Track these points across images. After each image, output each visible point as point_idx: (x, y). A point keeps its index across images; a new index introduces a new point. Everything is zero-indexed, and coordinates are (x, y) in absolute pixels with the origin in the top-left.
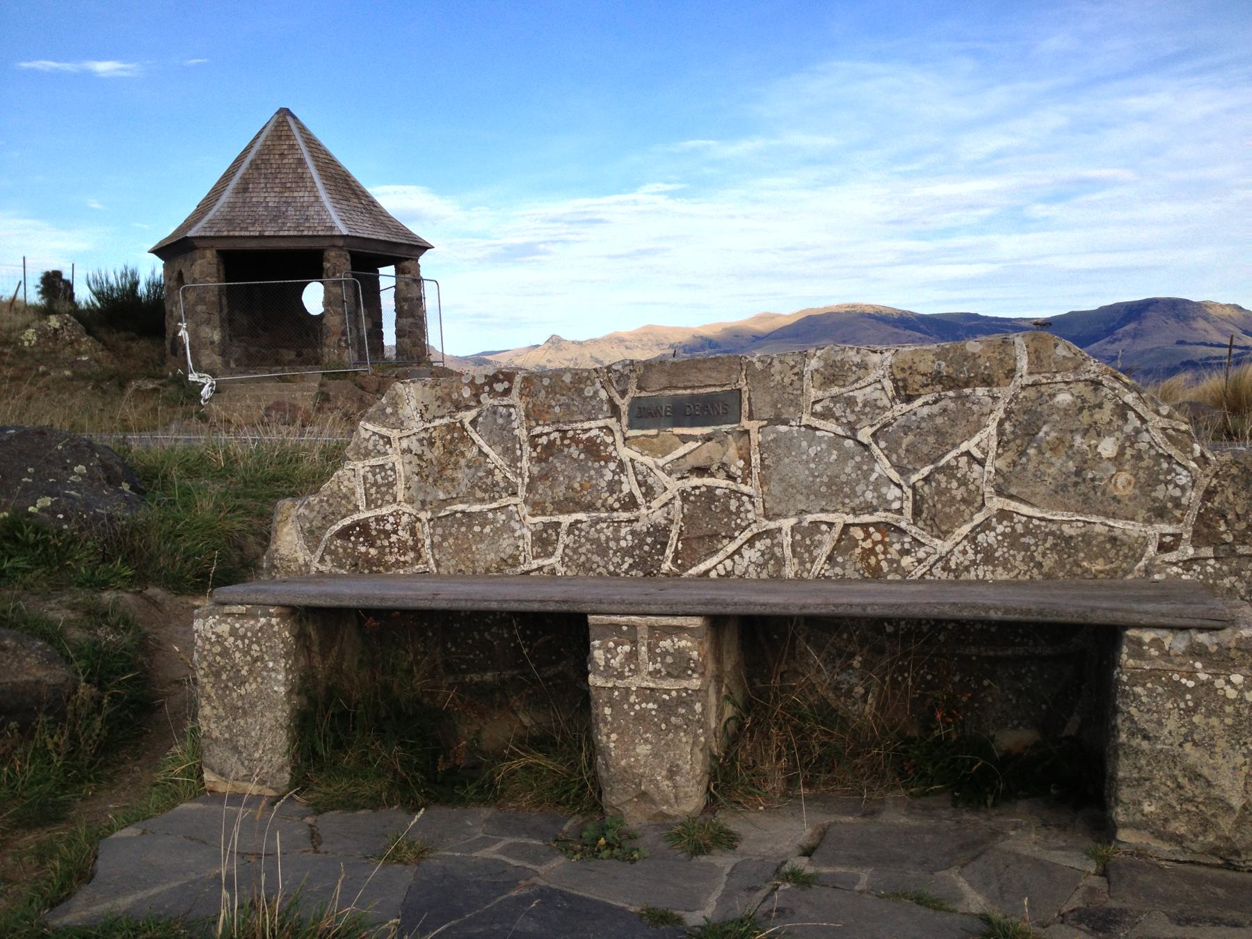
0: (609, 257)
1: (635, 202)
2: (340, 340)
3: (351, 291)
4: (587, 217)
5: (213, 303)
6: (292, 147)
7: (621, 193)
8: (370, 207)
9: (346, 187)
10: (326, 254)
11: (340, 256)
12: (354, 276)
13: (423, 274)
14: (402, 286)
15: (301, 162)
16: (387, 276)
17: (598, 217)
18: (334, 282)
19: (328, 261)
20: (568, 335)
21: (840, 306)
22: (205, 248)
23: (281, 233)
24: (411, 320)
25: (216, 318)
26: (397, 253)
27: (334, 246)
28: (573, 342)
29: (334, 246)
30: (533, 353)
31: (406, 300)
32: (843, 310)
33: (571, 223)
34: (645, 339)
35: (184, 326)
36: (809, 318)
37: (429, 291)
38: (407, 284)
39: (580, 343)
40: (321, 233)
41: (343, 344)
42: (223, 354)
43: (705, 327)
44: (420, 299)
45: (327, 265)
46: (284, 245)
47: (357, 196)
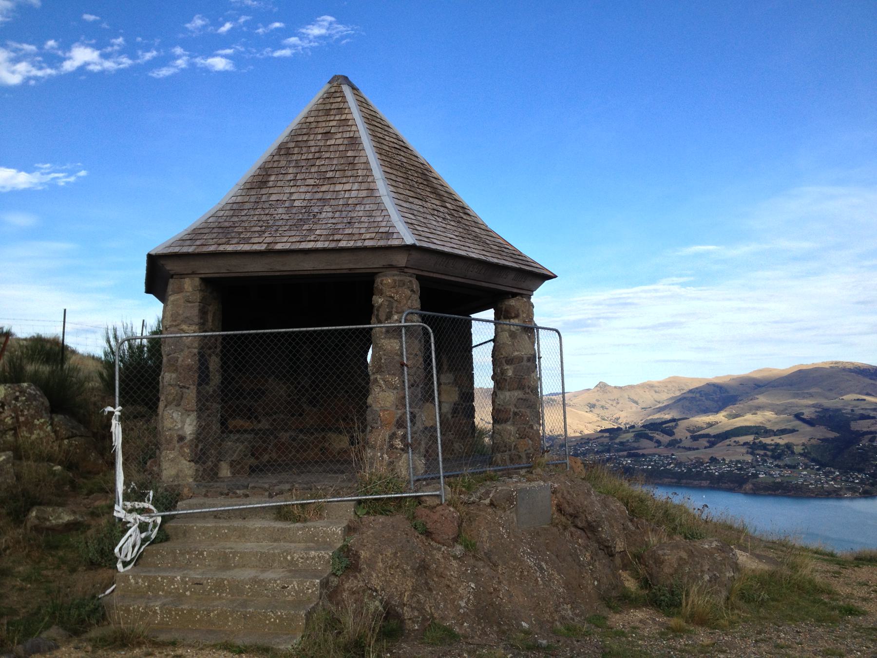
0: (639, 328)
1: (656, 291)
2: (393, 436)
3: (417, 346)
4: (621, 301)
5: (189, 368)
6: (344, 122)
7: (646, 285)
8: (460, 214)
9: (416, 179)
10: (378, 280)
11: (403, 284)
12: (424, 319)
13: (538, 320)
14: (505, 337)
15: (354, 142)
16: (483, 328)
17: (629, 301)
18: (388, 330)
19: (381, 293)
20: (612, 382)
21: (826, 363)
22: (182, 276)
23: (304, 246)
24: (517, 394)
25: (191, 394)
26: (504, 283)
27: (391, 267)
28: (615, 387)
29: (391, 267)
30: (586, 395)
31: (510, 361)
32: (827, 366)
33: (609, 305)
34: (670, 386)
35: (117, 411)
36: (800, 371)
37: (546, 344)
38: (513, 335)
39: (620, 388)
40: (368, 243)
41: (398, 443)
42: (198, 458)
43: (717, 377)
44: (533, 360)
45: (378, 300)
46: (308, 265)
47: (440, 197)
